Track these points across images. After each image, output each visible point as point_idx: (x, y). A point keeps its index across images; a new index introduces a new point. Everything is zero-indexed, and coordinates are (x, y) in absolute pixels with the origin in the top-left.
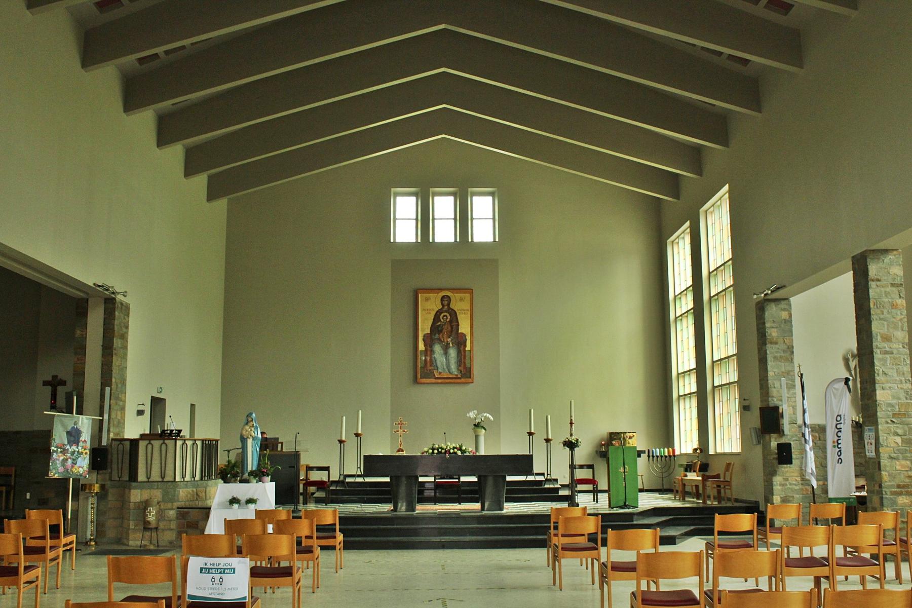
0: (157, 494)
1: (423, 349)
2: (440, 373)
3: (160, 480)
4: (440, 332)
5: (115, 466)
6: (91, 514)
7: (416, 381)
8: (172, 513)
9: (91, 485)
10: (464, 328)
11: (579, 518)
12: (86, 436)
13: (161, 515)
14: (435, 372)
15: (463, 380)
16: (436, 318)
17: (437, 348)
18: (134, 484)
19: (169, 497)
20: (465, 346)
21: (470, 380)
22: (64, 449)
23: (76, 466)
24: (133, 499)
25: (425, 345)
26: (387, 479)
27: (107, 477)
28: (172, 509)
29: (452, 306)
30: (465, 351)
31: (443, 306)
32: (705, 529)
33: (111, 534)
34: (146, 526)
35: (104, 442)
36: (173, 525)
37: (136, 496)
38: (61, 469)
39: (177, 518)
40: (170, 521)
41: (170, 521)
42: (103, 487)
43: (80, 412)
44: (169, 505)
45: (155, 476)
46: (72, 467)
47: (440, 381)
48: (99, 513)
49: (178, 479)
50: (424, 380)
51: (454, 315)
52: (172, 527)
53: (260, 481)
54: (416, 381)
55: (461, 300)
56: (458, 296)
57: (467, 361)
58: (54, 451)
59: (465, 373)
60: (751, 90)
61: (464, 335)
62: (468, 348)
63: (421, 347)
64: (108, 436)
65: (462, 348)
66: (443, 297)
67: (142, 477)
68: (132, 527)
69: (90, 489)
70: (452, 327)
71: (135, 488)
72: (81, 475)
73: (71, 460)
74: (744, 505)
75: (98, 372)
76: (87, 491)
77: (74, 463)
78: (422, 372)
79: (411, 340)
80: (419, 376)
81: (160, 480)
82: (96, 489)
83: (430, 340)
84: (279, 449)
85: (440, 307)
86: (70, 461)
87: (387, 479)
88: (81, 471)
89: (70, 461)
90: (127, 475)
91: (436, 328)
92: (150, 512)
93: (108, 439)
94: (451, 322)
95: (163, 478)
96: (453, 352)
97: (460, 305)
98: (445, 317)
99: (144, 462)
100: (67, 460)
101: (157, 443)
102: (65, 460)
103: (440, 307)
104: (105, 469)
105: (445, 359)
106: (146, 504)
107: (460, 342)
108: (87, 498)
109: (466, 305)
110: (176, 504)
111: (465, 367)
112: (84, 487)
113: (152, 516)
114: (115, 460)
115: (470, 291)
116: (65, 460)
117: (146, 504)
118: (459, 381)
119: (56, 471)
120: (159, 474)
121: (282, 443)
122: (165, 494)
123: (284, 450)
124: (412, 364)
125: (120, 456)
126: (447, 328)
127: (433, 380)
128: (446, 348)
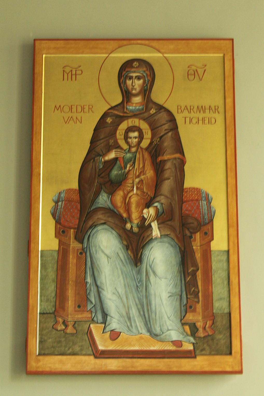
1: (54, 244)
2: (115, 335)
4: (113, 186)
7: (22, 365)
10: (203, 174)
14: (96, 329)
15: (201, 362)
16: (103, 135)
17: (106, 243)
21: (226, 362)
25: (61, 232)
29: (159, 95)
30: (207, 253)
31: (127, 95)
47: (113, 364)
55: (193, 74)
57: (218, 290)
60: (129, 92)
61: (200, 196)
62: (219, 243)
63: (46, 238)
65: (197, 244)
66: (128, 65)
70: (159, 168)
74: (198, 256)
79: (223, 100)
80: (35, 345)
85: (117, 98)
91: (97, 176)
94: (155, 151)
96: (160, 256)
98: (134, 136)
103: (117, 98)
105: (137, 292)
107: (188, 224)
111: (210, 315)
118: (186, 364)
124: (227, 230)
127: (89, 362)
128: (135, 245)
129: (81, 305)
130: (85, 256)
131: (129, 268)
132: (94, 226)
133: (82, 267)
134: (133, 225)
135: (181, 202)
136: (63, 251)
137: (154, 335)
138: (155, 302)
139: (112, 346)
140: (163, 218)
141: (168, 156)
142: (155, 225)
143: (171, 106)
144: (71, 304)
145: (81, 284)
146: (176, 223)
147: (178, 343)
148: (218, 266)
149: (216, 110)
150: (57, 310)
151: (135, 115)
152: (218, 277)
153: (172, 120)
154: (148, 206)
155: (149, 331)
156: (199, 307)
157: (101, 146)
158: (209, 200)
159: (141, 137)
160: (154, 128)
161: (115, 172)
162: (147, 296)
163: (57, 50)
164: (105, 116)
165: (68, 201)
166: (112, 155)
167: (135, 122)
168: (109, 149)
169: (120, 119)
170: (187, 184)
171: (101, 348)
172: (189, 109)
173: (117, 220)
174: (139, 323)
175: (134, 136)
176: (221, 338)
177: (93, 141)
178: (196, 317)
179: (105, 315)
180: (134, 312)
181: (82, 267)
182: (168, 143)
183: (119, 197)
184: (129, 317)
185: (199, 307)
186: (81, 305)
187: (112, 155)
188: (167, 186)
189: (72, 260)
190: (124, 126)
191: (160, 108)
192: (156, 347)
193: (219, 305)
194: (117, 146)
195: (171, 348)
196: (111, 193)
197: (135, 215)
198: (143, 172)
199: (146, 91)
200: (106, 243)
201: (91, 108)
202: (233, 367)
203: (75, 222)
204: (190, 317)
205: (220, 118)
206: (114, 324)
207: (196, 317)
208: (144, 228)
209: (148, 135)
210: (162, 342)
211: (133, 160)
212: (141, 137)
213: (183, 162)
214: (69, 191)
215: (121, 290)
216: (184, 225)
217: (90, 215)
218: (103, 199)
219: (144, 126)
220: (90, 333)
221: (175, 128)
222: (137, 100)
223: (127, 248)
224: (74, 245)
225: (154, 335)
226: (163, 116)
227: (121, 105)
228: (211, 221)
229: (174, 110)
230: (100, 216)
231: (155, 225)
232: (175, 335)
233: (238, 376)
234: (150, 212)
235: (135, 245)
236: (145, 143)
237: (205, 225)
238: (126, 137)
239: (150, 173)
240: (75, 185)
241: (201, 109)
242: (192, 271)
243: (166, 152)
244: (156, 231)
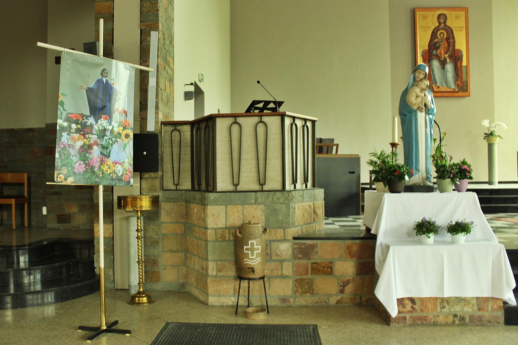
0: (256, 214)
2: (438, 87)
3: (257, 187)
4: (437, 48)
5: (167, 165)
6: (135, 248)
8: (285, 248)
9: (135, 199)
10: (460, 45)
12: (123, 99)
13: (268, 255)
15: (460, 94)
16: (434, 34)
18: (212, 196)
19: (275, 222)
20: (462, 62)
21: (466, 94)
22: (84, 126)
23: (109, 161)
24: (211, 223)
26: (47, 183)
27: (157, 182)
28: (285, 240)
31: (440, 24)
33: (169, 277)
34: (242, 273)
35: (151, 127)
36: (288, 269)
37: (218, 217)
38: (79, 167)
39: (295, 257)
40: (282, 261)
41: (282, 261)
42: (155, 201)
43: (109, 53)
44: (280, 234)
45: (249, 181)
46: (102, 162)
48: (148, 242)
49: (289, 186)
51: (450, 32)
52: (285, 273)
55: (457, 17)
56: (454, 13)
57: (464, 76)
58: (63, 129)
61: (460, 51)
62: (464, 63)
64: (157, 118)
65: (459, 64)
66: (439, 16)
67: (223, 182)
68: (212, 271)
69: (134, 205)
70: (449, 44)
71: (216, 203)
72: (120, 179)
73: (92, 152)
74: (459, 67)
76: (129, 208)
77: (105, 155)
81: (257, 187)
82: (145, 204)
83: (428, 57)
84: (334, 152)
85: (437, 25)
86: (96, 151)
87: (47, 183)
88: (119, 170)
89: (96, 151)
90: (189, 180)
92: (252, 250)
93: (157, 122)
94: (447, 39)
95: (262, 185)
96: (449, 67)
97: (455, 22)
98: (442, 35)
99: (227, 156)
100: (90, 147)
101: (248, 123)
102: (86, 149)
104: (156, 170)
106: (238, 237)
107: (456, 57)
108: (127, 219)
109: (462, 23)
110: (293, 232)
112: (122, 201)
113: (254, 258)
114: (167, 158)
115: (466, 10)
116: (86, 149)
117: (238, 237)
118: (456, 94)
119: (68, 172)
120: (228, 180)
121: (337, 145)
122: (271, 213)
123: (339, 153)
125: (176, 150)
126: (444, 45)
128: (443, 64)
131: (442, 70)
132: (432, 59)
133: (203, 154)
134: (442, 59)
135: (455, 52)
137: (448, 87)
139: (438, 90)
140: (450, 57)
142: (448, 59)
143: (451, 27)
146: (453, 58)
147: (454, 89)
151: (442, 29)
153: (452, 31)
154: (446, 53)
155: (447, 86)
156: (459, 80)
157: (433, 38)
158: (461, 52)
159: (444, 35)
161: (437, 45)
162: (446, 77)
163: (421, 11)
164: (434, 29)
166: (436, 40)
167: (442, 31)
168: (435, 38)
169: (438, 30)
170: (456, 48)
171: (435, 90)
172: (456, 27)
173: (438, 57)
176: (465, 88)
177: (431, 36)
178: (459, 83)
179: (436, 82)
180: (443, 81)
181: (203, 154)
182: (451, 36)
183: (439, 51)
185: (459, 80)
187: (436, 40)
188: (451, 48)
191: (449, 27)
192: (449, 90)
193: (464, 80)
194: (437, 38)
195: (452, 90)
196: (437, 50)
197: (443, 56)
198: (444, 45)
199: (445, 22)
200: (436, 63)
201: (430, 27)
202: (188, 146)
203: (428, 58)
204: (457, 83)
205: (464, 30)
206: (438, 84)
207: (459, 83)
211: (442, 41)
213: (455, 42)
214: (426, 50)
215: (440, 76)
216: (455, 59)
217: (431, 57)
218: (434, 52)
219: (445, 32)
222: (442, 25)
223: (441, 65)
225: (448, 87)
227: (438, 27)
228: (462, 58)
229: (452, 28)
231: (448, 59)
232: (453, 87)
233: (468, 98)
234: (446, 56)
235: (443, 64)
236: (445, 37)
237: (461, 59)
239: (446, 45)
240: (427, 48)
241: (459, 27)
242: (457, 70)
244: (448, 60)
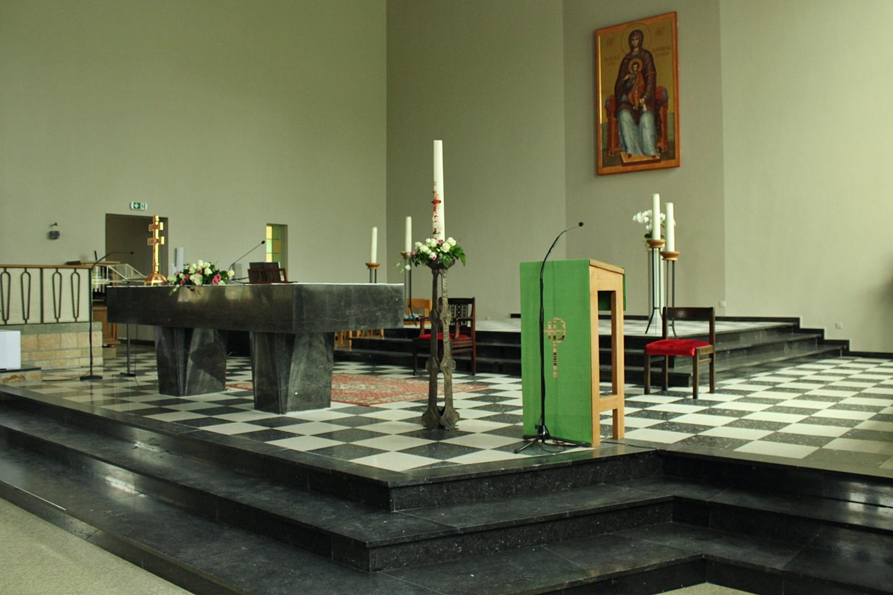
2: (630, 156)
4: (627, 90)
11: (333, 346)
14: (622, 154)
15: (663, 164)
16: (624, 69)
17: (626, 117)
20: (666, 107)
21: (672, 162)
30: (665, 116)
31: (632, 48)
32: (508, 365)
47: (629, 168)
50: (607, 170)
53: (373, 373)
54: (599, 174)
57: (670, 131)
59: (667, 153)
62: (670, 110)
65: (661, 112)
74: (662, 117)
75: (817, 402)
78: (610, 157)
79: (592, 106)
85: (628, 51)
91: (622, 88)
94: (644, 72)
96: (647, 120)
98: (635, 67)
103: (628, 51)
105: (637, 134)
118: (657, 165)
124: (593, 144)
127: (620, 168)
128: (637, 116)
129: (617, 145)
130: (618, 124)
131: (635, 127)
136: (610, 123)
137: (645, 154)
138: (645, 139)
139: (629, 161)
140: (647, 102)
141: (650, 73)
142: (644, 106)
144: (613, 145)
145: (617, 135)
147: (654, 157)
148: (670, 119)
149: (668, 48)
150: (607, 150)
151: (636, 57)
152: (670, 125)
153: (651, 56)
154: (641, 97)
155: (643, 152)
158: (666, 92)
160: (643, 62)
161: (628, 85)
162: (642, 137)
165: (611, 101)
166: (627, 77)
168: (625, 75)
170: (658, 85)
171: (625, 161)
173: (629, 106)
174: (639, 150)
175: (635, 67)
179: (626, 148)
180: (637, 145)
182: (649, 67)
183: (630, 96)
184: (775, 338)
186: (617, 145)
187: (627, 77)
188: (649, 87)
189: (613, 126)
190: (631, 63)
191: (646, 51)
192: (645, 159)
193: (670, 138)
194: (629, 73)
195: (651, 159)
196: (627, 94)
197: (637, 103)
199: (640, 45)
200: (626, 117)
204: (659, 145)
206: (630, 151)
208: (641, 107)
209: (641, 65)
210: (396, 485)
211: (635, 78)
212: (638, 67)
213: (655, 75)
218: (624, 98)
219: (640, 61)
220: (620, 156)
221: (652, 60)
222: (636, 50)
224: (614, 119)
225: (645, 154)
226: (647, 55)
227: (630, 54)
228: (667, 101)
230: (623, 105)
231: (644, 106)
232: (652, 153)
234: (642, 100)
235: (637, 116)
238: (633, 67)
239: (642, 83)
240: (613, 93)
241: (663, 49)
243: (648, 72)
244: (645, 109)
